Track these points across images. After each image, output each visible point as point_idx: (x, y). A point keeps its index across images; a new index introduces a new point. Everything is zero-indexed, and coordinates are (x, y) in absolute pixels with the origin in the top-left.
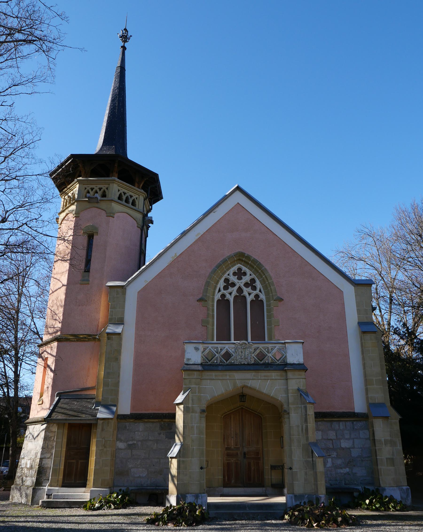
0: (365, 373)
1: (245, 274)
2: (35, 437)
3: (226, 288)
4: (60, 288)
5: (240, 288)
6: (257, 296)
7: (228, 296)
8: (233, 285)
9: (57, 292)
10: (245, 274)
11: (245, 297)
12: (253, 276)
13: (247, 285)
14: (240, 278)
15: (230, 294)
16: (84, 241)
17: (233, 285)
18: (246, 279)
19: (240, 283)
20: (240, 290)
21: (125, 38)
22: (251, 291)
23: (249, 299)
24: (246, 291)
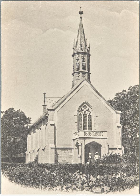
0: (89, 45)
1: (86, 107)
2: (58, 151)
3: (81, 111)
4: (83, 81)
5: (85, 111)
6: (90, 114)
7: (82, 114)
8: (83, 110)
9: (74, 95)
10: (86, 107)
11: (86, 114)
12: (89, 108)
13: (87, 110)
14: (85, 108)
15: (83, 113)
16: (44, 118)
17: (83, 110)
18: (87, 109)
19: (85, 110)
20: (85, 112)
21: (81, 7)
22: (88, 112)
23: (88, 115)
24: (87, 112)
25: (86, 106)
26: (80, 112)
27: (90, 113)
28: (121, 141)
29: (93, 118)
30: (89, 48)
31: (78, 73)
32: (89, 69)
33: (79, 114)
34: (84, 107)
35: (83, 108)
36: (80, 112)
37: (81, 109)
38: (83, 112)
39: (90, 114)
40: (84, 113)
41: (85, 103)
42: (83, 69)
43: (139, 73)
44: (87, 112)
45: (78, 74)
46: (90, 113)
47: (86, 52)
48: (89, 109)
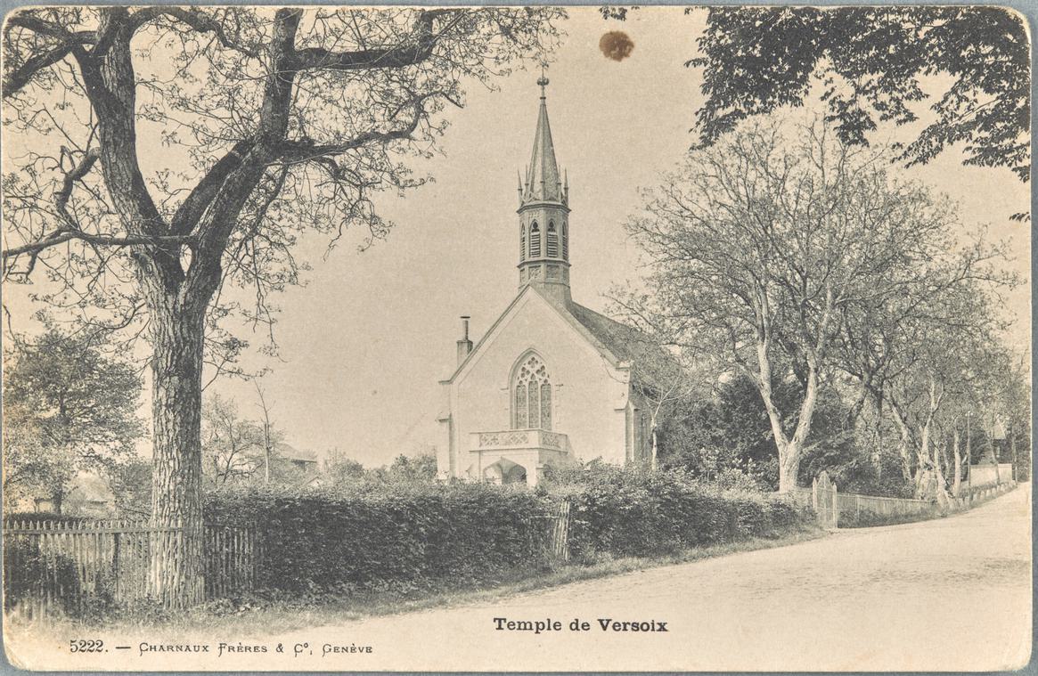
6: (546, 381)
13: (538, 372)
17: (528, 372)
18: (538, 367)
19: (533, 371)
25: (536, 358)
26: (521, 379)
27: (545, 377)
28: (1032, 202)
29: (554, 388)
30: (566, 189)
31: (535, 265)
32: (565, 256)
33: (516, 383)
34: (529, 363)
35: (528, 367)
36: (521, 379)
37: (523, 369)
38: (528, 377)
39: (546, 381)
40: (529, 380)
41: (530, 352)
42: (548, 253)
43: (888, 670)
44: (538, 376)
45: (536, 267)
46: (545, 377)
47: (560, 204)
48: (543, 367)
